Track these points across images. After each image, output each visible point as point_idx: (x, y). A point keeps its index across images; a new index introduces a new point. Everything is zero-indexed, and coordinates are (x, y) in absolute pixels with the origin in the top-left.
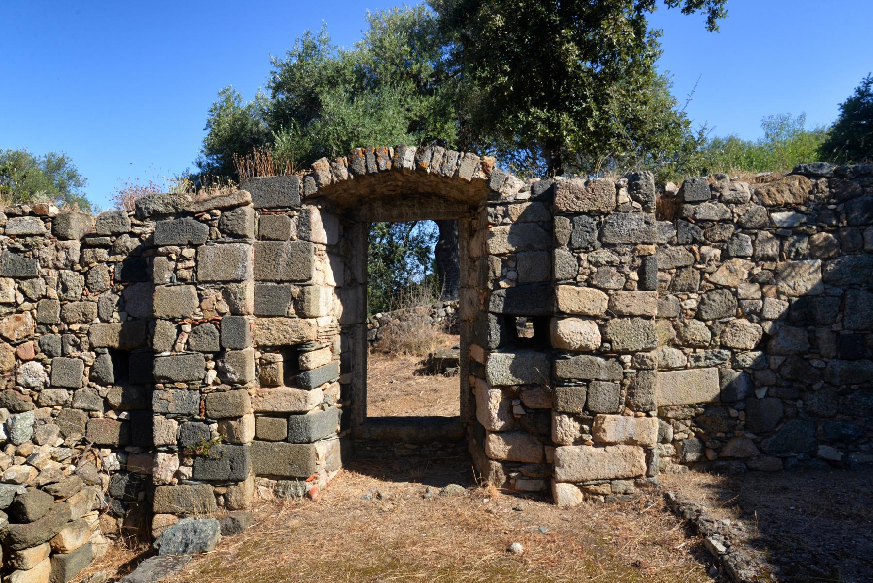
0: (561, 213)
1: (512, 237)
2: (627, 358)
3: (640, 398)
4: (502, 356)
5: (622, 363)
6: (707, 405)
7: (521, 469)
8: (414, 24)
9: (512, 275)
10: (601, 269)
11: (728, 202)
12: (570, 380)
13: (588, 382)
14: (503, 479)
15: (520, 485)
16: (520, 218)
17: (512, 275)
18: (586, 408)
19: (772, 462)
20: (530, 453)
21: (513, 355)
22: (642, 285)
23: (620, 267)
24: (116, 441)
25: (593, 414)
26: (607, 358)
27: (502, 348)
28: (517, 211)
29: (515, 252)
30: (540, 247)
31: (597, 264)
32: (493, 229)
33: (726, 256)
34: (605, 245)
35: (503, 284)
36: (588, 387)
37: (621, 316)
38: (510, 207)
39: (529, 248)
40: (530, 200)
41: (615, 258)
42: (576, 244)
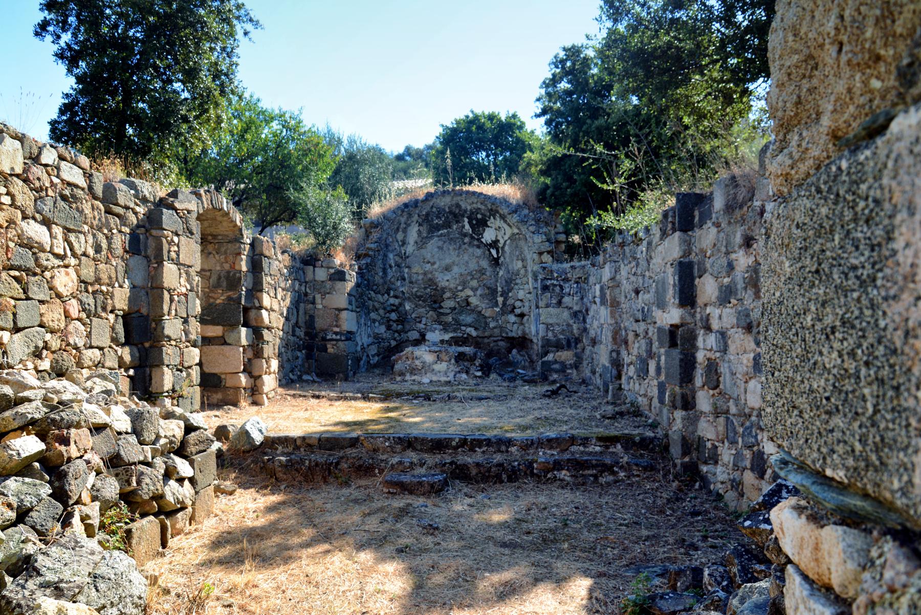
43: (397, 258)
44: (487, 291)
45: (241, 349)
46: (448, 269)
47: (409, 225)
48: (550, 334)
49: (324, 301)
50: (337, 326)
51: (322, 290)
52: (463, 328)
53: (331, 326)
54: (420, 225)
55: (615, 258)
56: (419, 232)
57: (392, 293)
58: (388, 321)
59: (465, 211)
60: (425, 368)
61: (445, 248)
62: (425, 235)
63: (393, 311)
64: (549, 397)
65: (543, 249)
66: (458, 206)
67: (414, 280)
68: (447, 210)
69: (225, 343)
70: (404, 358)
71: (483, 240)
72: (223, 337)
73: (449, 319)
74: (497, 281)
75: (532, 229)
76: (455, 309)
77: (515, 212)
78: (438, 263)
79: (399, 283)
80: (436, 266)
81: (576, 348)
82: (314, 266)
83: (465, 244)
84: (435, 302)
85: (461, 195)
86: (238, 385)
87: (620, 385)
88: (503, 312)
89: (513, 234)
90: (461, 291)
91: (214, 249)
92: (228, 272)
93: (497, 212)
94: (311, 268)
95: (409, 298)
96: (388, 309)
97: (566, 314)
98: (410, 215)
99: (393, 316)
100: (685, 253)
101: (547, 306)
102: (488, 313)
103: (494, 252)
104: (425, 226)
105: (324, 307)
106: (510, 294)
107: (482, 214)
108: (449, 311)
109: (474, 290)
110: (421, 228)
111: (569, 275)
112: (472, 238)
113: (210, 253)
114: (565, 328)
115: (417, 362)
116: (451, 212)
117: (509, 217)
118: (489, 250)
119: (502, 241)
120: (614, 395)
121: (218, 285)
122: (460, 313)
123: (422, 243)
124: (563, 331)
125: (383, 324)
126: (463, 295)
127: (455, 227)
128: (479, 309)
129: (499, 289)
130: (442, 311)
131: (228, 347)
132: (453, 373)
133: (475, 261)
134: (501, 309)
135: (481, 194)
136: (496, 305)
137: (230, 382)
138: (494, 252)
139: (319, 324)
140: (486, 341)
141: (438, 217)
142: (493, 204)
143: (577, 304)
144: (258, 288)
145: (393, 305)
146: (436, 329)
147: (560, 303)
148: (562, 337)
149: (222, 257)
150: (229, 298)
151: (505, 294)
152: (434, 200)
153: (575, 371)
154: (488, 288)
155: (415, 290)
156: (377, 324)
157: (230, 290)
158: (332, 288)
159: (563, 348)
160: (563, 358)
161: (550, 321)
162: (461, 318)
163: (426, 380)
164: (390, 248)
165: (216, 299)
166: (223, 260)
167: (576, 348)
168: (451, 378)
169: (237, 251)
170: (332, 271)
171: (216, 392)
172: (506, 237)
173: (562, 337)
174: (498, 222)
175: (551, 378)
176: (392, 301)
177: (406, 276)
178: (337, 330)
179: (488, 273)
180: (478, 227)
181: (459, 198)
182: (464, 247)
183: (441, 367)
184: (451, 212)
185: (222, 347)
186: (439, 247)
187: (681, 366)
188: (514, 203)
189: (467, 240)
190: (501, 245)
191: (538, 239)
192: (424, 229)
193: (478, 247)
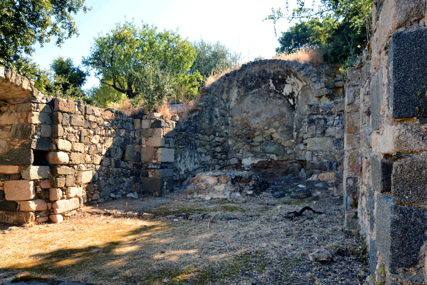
0: (60, 111)
1: (40, 117)
2: (76, 167)
3: (79, 181)
4: (35, 167)
5: (74, 168)
6: (89, 183)
7: (40, 214)
8: (221, 46)
9: (39, 133)
10: (70, 134)
11: (96, 116)
12: (61, 175)
13: (66, 175)
14: (34, 218)
15: (41, 220)
16: (42, 110)
17: (39, 133)
18: (65, 186)
19: (102, 200)
20: (44, 206)
21: (38, 167)
22: (80, 141)
23: (75, 134)
24: (58, 169)
25: (67, 187)
26: (70, 167)
27: (34, 164)
28: (42, 107)
29: (41, 124)
30: (48, 123)
31: (69, 132)
32: (33, 113)
33: (95, 134)
34: (72, 126)
35: (36, 137)
36: (66, 177)
37: (75, 152)
38: (39, 104)
39: (45, 123)
40: (46, 103)
41: (74, 130)
42: (64, 124)
43: (222, 111)
44: (285, 129)
45: (32, 183)
46: (258, 115)
47: (231, 88)
48: (315, 159)
49: (147, 142)
50: (155, 159)
51: (146, 135)
52: (268, 155)
53: (151, 159)
54: (239, 88)
55: (354, 82)
56: (239, 92)
57: (217, 134)
58: (214, 153)
59: (270, 74)
60: (209, 189)
61: (256, 102)
62: (243, 94)
63: (218, 146)
64: (291, 218)
65: (321, 93)
66: (264, 71)
67: (235, 125)
68: (257, 75)
69: (21, 178)
70: (196, 181)
71: (284, 93)
72: (19, 174)
73: (258, 149)
74: (293, 121)
75: (314, 79)
76: (263, 142)
77: (302, 69)
78: (251, 112)
79: (223, 127)
80: (250, 114)
81: (337, 170)
82: (141, 119)
83: (270, 97)
84: (249, 138)
85: (266, 63)
86: (27, 210)
87: (356, 213)
88: (297, 143)
89: (304, 86)
90: (267, 130)
91: (14, 109)
92: (23, 125)
93: (292, 72)
94: (139, 120)
95: (232, 137)
96: (214, 145)
97: (329, 142)
98: (231, 82)
99: (218, 149)
100: (408, 16)
101: (313, 136)
102: (286, 144)
103: (291, 101)
104: (242, 88)
105: (147, 146)
106: (301, 130)
107: (281, 75)
108: (258, 144)
109: (276, 128)
110: (240, 90)
111: (332, 110)
112: (276, 92)
113: (12, 112)
114: (328, 153)
115: (202, 184)
116: (260, 76)
117: (298, 73)
118: (288, 100)
119: (296, 93)
120: (349, 224)
121: (15, 136)
122: (266, 145)
123: (240, 100)
124: (326, 157)
125: (208, 155)
126: (268, 132)
127: (263, 86)
128: (280, 141)
129: (295, 126)
130: (253, 144)
131: (23, 181)
132: (229, 192)
133: (277, 108)
134: (296, 140)
135: (280, 60)
136: (292, 137)
137: (23, 208)
138: (291, 101)
139: (144, 158)
140: (284, 163)
141: (251, 81)
142: (287, 66)
143: (338, 133)
144: (55, 136)
145: (219, 142)
146: (249, 156)
147: (324, 133)
148: (325, 161)
149: (19, 114)
150: (23, 145)
151: (298, 130)
152: (247, 69)
153: (335, 189)
154: (287, 127)
155: (236, 131)
156: (203, 155)
157: (24, 139)
158: (153, 133)
159: (326, 170)
160: (325, 178)
161: (315, 148)
162: (267, 148)
163: (208, 198)
164: (216, 104)
165: (14, 146)
166: (19, 117)
167: (337, 170)
168: (227, 196)
169: (29, 109)
170: (153, 121)
171: (13, 215)
172: (299, 89)
173: (325, 161)
174: (293, 79)
175: (315, 195)
176: (217, 139)
177: (229, 122)
178: (155, 161)
179: (286, 116)
180: (280, 85)
181: (264, 66)
182: (269, 99)
183: (221, 187)
184: (260, 76)
185: (18, 181)
186: (252, 101)
187: (393, 234)
188: (303, 63)
189: (272, 94)
190: (296, 96)
191: (317, 86)
192: (242, 90)
193: (280, 98)
